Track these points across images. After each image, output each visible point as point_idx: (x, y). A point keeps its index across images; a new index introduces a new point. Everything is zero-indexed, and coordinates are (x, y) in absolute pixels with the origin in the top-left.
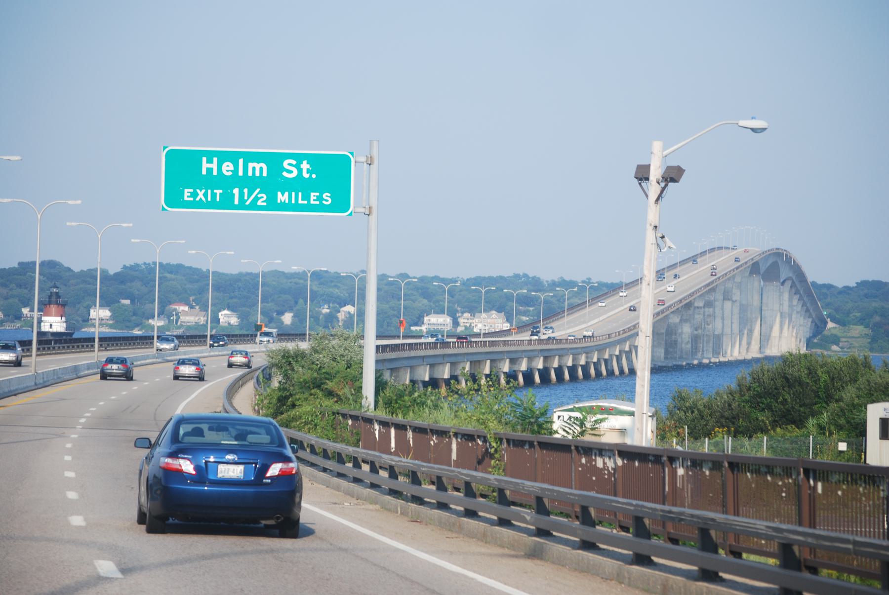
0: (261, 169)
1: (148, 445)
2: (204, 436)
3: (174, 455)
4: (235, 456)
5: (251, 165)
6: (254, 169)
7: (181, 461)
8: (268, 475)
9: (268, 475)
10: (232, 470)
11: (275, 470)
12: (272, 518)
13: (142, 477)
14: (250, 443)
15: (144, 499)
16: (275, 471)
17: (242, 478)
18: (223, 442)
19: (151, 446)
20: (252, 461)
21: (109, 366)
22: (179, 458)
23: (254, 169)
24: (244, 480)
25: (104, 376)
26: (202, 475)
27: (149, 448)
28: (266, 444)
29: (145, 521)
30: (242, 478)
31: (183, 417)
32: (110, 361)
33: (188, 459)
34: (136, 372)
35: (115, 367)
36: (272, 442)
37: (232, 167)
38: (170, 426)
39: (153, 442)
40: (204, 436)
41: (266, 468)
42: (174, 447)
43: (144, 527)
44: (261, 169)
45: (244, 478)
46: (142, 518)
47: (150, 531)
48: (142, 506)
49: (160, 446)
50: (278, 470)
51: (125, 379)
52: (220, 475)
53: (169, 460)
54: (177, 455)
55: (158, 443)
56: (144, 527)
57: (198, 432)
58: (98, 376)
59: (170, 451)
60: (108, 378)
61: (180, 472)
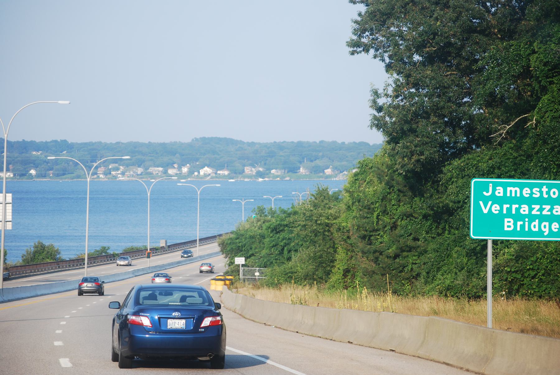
0: (516, 191)
1: (118, 307)
2: (157, 300)
3: (136, 314)
4: (179, 313)
5: (509, 189)
6: (511, 191)
7: (142, 318)
8: (203, 325)
9: (203, 325)
10: (177, 323)
11: (207, 322)
12: (206, 356)
13: (115, 330)
14: (189, 304)
15: (116, 344)
16: (206, 323)
17: (184, 328)
18: (170, 304)
19: (120, 307)
20: (191, 317)
21: (85, 284)
22: (140, 316)
23: (511, 191)
24: (186, 329)
25: (81, 293)
26: (157, 326)
27: (118, 308)
28: (200, 304)
29: (118, 360)
30: (184, 328)
31: (142, 287)
32: (85, 280)
33: (147, 317)
34: (106, 287)
35: (90, 285)
36: (203, 303)
37: (498, 208)
38: (133, 294)
39: (121, 304)
40: (157, 300)
41: (200, 320)
42: (137, 308)
43: (117, 364)
44: (516, 191)
45: (186, 328)
46: (115, 358)
47: (122, 366)
48: (115, 348)
49: (126, 307)
50: (209, 322)
51: (98, 294)
52: (169, 327)
53: (134, 318)
54: (139, 314)
55: (125, 305)
56: (117, 364)
57: (153, 297)
58: (76, 292)
59: (134, 311)
60: (84, 294)
61: (141, 325)
